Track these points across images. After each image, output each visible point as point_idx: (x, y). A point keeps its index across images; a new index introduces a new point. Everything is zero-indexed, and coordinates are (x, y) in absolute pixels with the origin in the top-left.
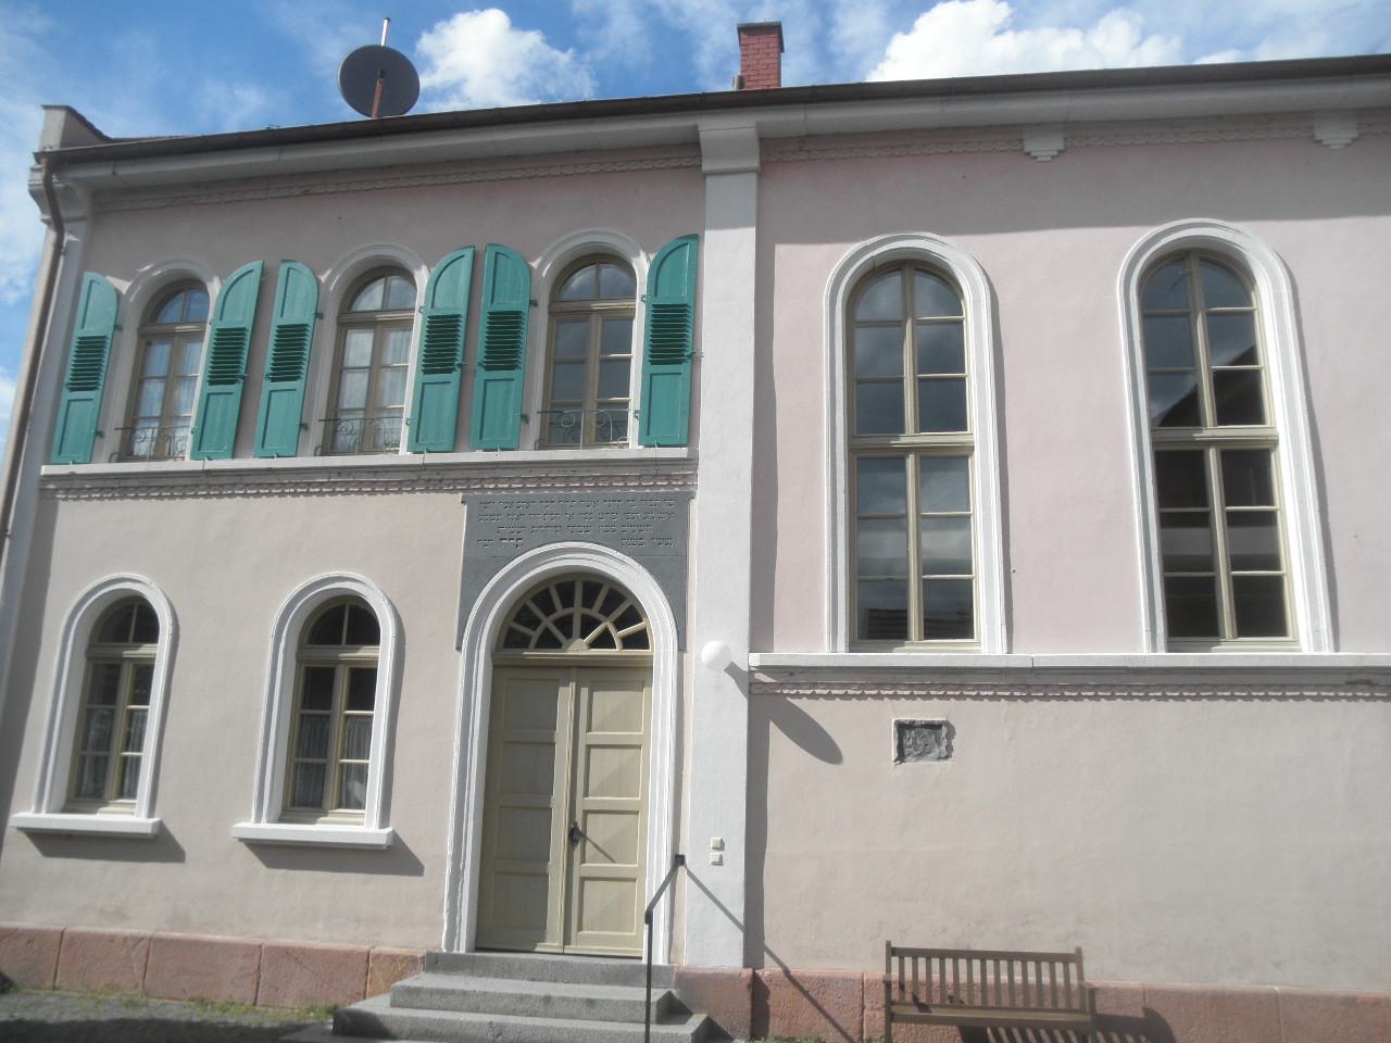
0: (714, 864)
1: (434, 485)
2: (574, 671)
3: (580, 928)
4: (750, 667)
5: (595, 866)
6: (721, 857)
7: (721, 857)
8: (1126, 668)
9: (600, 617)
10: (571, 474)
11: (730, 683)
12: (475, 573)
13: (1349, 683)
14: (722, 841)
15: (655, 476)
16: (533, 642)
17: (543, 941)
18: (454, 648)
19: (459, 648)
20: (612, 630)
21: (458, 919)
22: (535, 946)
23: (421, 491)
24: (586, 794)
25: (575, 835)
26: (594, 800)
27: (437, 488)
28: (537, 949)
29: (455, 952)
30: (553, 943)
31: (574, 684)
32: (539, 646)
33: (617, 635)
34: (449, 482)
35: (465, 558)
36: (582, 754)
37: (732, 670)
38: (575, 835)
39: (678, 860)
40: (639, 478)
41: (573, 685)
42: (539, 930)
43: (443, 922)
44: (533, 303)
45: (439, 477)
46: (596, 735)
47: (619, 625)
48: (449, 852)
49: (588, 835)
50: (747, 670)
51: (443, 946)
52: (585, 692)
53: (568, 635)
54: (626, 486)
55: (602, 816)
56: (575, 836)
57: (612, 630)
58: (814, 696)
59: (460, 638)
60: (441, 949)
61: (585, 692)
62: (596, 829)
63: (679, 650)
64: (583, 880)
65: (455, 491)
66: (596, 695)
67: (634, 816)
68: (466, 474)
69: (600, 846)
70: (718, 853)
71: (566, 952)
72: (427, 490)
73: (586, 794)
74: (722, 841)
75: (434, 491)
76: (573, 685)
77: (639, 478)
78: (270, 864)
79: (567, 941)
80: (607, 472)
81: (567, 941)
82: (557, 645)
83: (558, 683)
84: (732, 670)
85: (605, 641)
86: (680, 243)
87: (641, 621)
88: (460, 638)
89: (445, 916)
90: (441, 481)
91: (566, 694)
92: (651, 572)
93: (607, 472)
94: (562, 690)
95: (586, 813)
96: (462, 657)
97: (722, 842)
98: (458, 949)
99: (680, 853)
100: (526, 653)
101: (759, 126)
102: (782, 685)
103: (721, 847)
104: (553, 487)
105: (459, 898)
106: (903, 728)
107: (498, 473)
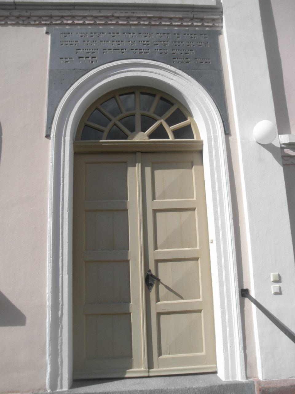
0: (276, 294)
1: (23, 21)
2: (138, 155)
3: (160, 354)
4: (281, 144)
5: (167, 303)
6: (280, 288)
7: (280, 288)
9: (156, 116)
10: (131, 15)
11: (268, 156)
12: (59, 81)
14: (279, 275)
15: (192, 19)
16: (105, 134)
17: (131, 368)
18: (44, 135)
19: (48, 136)
20: (165, 125)
21: (59, 360)
22: (125, 373)
23: (13, 25)
24: (156, 248)
26: (162, 252)
27: (26, 23)
28: (127, 375)
29: (58, 390)
30: (139, 367)
31: (140, 164)
32: (110, 137)
33: (169, 130)
34: (36, 18)
35: (51, 71)
36: (150, 217)
37: (269, 147)
38: (151, 280)
39: (244, 293)
40: (181, 19)
41: (139, 165)
42: (126, 357)
43: (46, 365)
45: (28, 14)
46: (160, 202)
47: (170, 122)
48: (48, 303)
49: (160, 277)
50: (279, 146)
51: (47, 386)
52: (148, 170)
53: (133, 130)
54: (171, 25)
55: (170, 264)
56: (150, 281)
57: (165, 125)
59: (49, 128)
60: (45, 390)
61: (148, 170)
62: (166, 274)
63: (226, 134)
64: (159, 314)
65: (40, 25)
66: (157, 172)
67: (193, 262)
68: (49, 13)
69: (170, 287)
70: (278, 285)
71: (151, 374)
72: (17, 24)
73: (156, 248)
74: (279, 275)
75: (23, 25)
76: (139, 165)
77: (181, 19)
79: (150, 365)
80: (157, 14)
81: (150, 365)
82: (126, 137)
83: (125, 165)
84: (269, 147)
87: (186, 119)
88: (49, 128)
89: (48, 359)
90: (29, 18)
91: (134, 173)
92: (198, 79)
93: (157, 14)
94: (130, 170)
95: (157, 262)
96: (51, 143)
97: (279, 276)
98: (61, 388)
99: (245, 288)
100: (101, 141)
103: (278, 280)
104: (117, 24)
105: (59, 341)
107: (75, 13)
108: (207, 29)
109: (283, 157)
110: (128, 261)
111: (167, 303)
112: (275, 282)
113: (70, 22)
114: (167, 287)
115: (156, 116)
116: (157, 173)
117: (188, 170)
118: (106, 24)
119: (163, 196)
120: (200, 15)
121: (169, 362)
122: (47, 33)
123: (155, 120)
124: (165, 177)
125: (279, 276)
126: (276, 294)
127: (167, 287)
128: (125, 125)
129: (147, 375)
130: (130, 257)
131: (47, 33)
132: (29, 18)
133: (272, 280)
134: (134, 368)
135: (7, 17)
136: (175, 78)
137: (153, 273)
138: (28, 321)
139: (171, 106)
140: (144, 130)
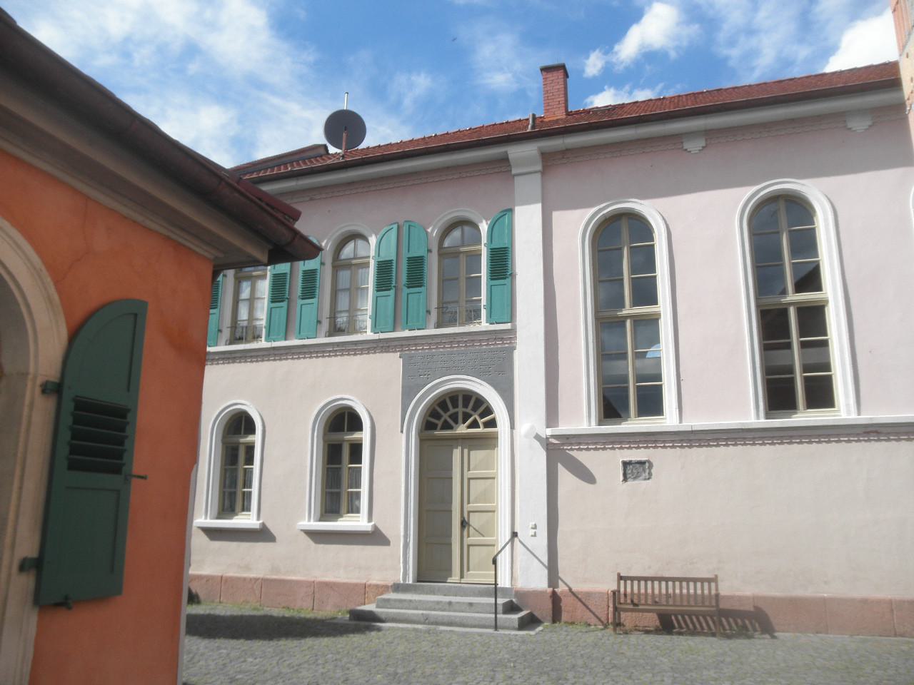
0: (532, 536)
3: (468, 570)
5: (474, 539)
6: (535, 533)
8: (742, 429)
9: (472, 412)
11: (537, 444)
12: (408, 393)
13: (865, 433)
19: (402, 432)
25: (464, 524)
26: (473, 506)
28: (567, 588)
30: (455, 578)
36: (466, 482)
37: (537, 437)
38: (464, 524)
39: (514, 535)
41: (460, 448)
44: (429, 251)
46: (473, 473)
49: (471, 523)
51: (401, 579)
52: (466, 451)
53: (456, 422)
58: (579, 449)
61: (466, 451)
62: (475, 520)
65: (396, 351)
69: (477, 528)
70: (534, 531)
72: (382, 352)
73: (469, 503)
76: (460, 448)
78: (317, 542)
79: (462, 577)
81: (462, 577)
82: (451, 428)
84: (537, 437)
85: (475, 424)
86: (502, 214)
90: (389, 347)
91: (457, 453)
94: (455, 451)
95: (469, 512)
96: (404, 436)
97: (535, 525)
101: (539, 148)
102: (563, 444)
103: (535, 527)
106: (626, 464)
107: (418, 341)
108: (507, 345)
109: (547, 445)
110: (451, 511)
111: (474, 539)
112: (532, 528)
113: (414, 348)
114: (474, 529)
115: (472, 412)
116: (472, 453)
117: (492, 451)
118: (437, 348)
119: (475, 469)
120: (500, 336)
121: (473, 576)
122: (400, 357)
123: (471, 416)
124: (477, 455)
125: (535, 525)
126: (532, 536)
127: (474, 529)
128: (475, 402)
129: (458, 581)
130: (453, 509)
131: (400, 357)
132: (389, 347)
133: (530, 526)
134: (220, 345)
135: (375, 348)
136: (481, 387)
137: (466, 519)
138: (391, 543)
139: (479, 405)
140: (464, 423)
